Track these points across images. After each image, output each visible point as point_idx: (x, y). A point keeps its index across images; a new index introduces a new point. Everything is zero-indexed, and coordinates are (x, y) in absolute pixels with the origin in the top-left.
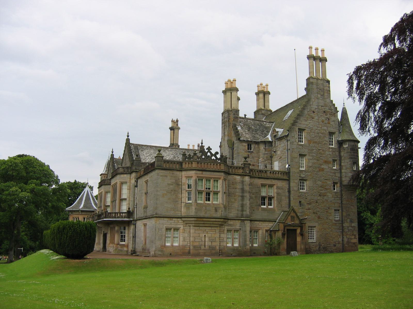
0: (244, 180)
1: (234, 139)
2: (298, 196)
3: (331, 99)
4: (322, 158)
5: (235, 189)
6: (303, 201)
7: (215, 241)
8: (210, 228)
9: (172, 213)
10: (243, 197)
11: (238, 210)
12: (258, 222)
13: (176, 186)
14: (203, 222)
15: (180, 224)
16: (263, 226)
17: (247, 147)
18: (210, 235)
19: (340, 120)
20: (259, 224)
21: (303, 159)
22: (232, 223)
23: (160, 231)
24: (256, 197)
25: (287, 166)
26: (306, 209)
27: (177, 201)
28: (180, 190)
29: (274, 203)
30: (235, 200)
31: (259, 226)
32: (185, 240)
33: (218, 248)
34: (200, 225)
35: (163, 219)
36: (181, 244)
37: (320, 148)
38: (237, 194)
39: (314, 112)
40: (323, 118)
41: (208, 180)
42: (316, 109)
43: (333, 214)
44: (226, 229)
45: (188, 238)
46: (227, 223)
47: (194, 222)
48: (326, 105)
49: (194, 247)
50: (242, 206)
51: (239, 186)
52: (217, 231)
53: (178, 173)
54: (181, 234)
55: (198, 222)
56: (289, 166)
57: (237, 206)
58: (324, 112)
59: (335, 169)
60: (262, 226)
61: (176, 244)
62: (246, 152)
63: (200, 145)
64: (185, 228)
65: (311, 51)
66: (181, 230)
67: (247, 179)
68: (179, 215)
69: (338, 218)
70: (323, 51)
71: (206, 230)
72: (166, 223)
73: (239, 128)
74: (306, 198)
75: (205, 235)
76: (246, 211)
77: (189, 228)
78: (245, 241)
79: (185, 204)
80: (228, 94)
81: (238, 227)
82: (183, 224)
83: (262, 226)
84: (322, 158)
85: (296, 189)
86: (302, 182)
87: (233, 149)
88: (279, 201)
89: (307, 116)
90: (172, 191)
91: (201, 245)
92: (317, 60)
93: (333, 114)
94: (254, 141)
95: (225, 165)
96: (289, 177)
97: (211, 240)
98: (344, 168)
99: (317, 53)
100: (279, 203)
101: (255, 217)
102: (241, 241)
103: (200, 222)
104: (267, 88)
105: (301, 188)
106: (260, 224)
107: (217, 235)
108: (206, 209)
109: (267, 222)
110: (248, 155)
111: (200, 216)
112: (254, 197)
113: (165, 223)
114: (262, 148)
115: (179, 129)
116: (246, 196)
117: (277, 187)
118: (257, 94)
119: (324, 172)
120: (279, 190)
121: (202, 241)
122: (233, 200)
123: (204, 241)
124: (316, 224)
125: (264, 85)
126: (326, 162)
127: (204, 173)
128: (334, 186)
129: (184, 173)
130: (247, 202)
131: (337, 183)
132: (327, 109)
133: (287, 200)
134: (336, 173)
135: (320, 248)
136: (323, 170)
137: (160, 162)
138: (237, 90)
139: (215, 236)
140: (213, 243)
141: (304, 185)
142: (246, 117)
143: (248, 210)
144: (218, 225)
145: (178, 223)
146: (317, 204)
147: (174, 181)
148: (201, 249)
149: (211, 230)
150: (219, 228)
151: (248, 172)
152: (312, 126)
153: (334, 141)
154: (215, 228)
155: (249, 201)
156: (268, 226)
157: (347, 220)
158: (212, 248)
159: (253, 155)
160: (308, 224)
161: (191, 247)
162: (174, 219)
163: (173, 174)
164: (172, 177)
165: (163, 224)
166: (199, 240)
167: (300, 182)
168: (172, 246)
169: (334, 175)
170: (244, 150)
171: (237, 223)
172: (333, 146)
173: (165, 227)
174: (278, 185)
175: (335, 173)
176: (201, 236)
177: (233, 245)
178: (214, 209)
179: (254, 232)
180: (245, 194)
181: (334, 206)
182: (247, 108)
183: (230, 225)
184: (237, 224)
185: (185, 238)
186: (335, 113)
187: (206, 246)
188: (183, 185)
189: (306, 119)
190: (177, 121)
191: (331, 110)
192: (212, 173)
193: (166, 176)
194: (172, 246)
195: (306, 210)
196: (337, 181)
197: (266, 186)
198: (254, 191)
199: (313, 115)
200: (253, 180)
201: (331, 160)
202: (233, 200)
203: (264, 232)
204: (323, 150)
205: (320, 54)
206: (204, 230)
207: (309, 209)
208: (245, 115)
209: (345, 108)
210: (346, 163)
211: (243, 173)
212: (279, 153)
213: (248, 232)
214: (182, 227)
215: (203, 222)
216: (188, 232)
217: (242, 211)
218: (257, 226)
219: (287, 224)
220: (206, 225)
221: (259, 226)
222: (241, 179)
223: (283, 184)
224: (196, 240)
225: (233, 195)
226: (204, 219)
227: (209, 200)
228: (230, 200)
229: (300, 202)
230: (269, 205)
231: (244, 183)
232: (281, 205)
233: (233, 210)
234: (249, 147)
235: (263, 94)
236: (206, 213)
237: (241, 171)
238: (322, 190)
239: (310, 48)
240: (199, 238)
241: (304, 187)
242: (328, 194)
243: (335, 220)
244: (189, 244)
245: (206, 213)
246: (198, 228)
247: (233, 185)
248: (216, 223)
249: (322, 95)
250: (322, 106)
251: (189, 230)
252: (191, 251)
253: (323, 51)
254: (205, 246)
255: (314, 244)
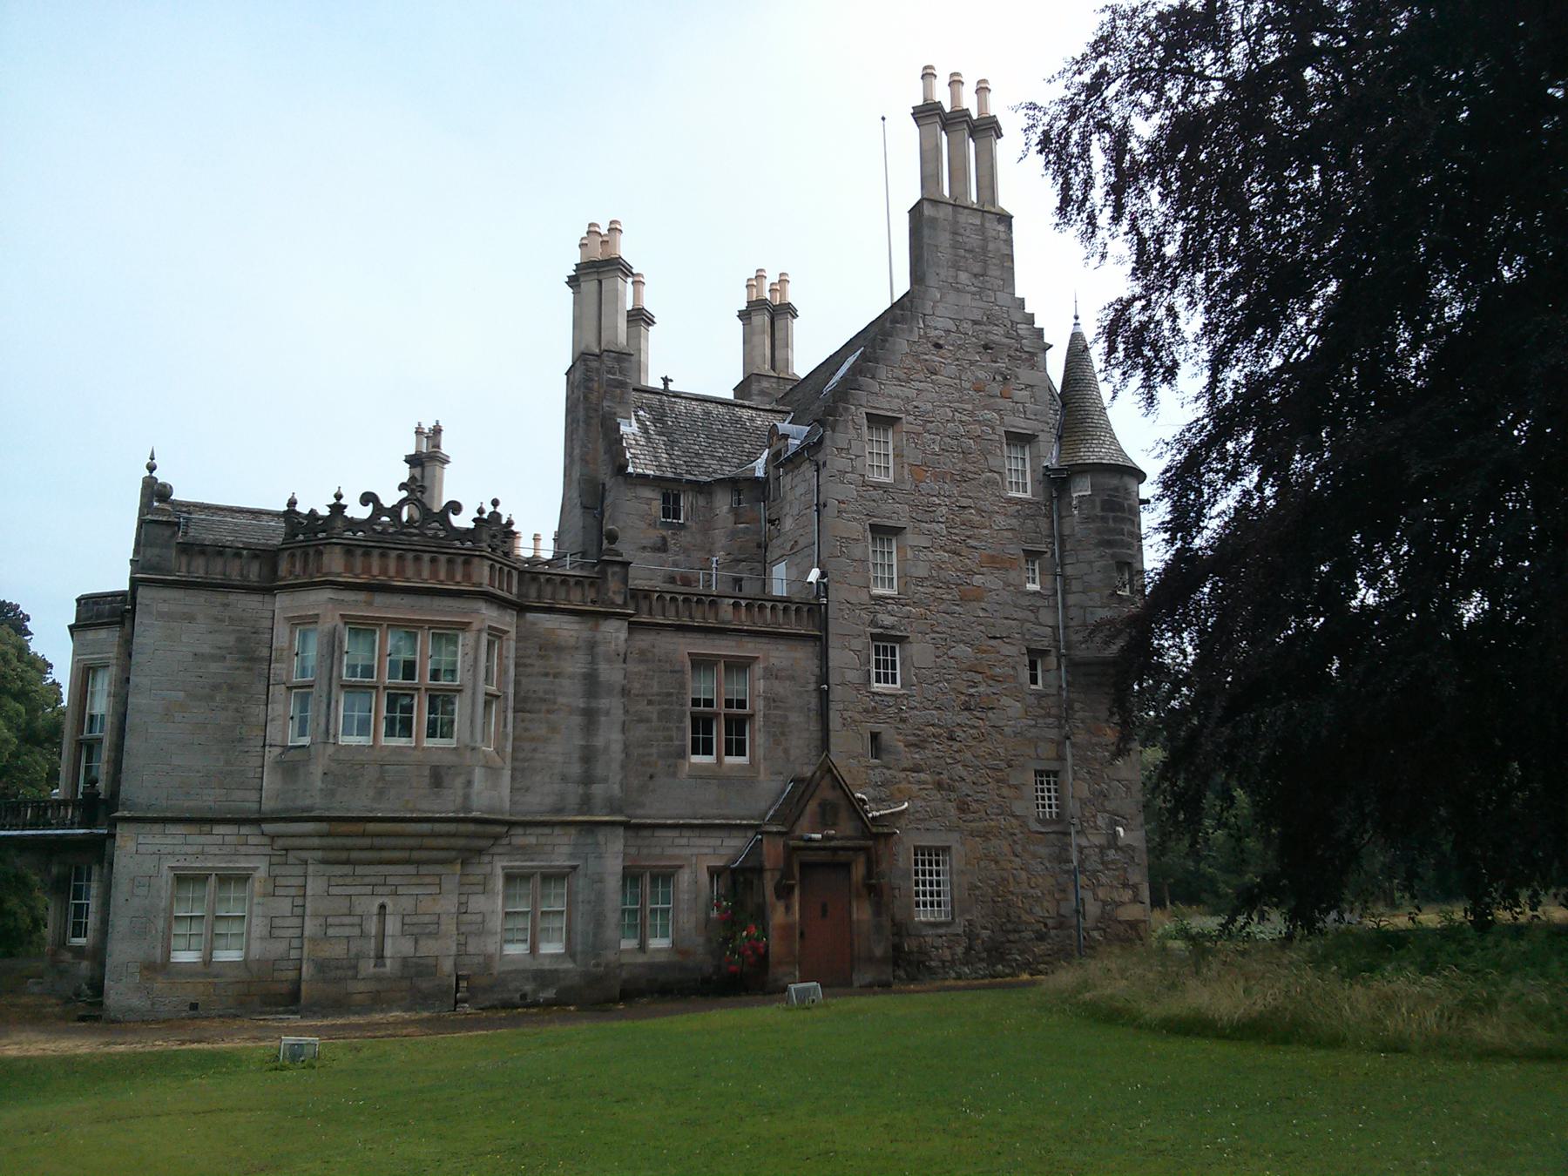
0: (599, 637)
1: (604, 474)
2: (866, 711)
3: (1017, 295)
4: (972, 542)
5: (550, 679)
6: (889, 735)
7: (434, 935)
8: (411, 869)
9: (208, 799)
10: (590, 717)
11: (564, 778)
12: (675, 833)
13: (238, 664)
14: (367, 842)
15: (252, 850)
16: (695, 851)
17: (657, 506)
18: (407, 904)
19: (1058, 386)
20: (677, 841)
21: (890, 546)
22: (533, 840)
23: (142, 891)
24: (664, 715)
25: (814, 575)
26: (904, 770)
27: (241, 740)
28: (261, 687)
29: (752, 740)
30: (553, 729)
31: (677, 851)
32: (277, 933)
33: (447, 966)
34: (355, 855)
35: (157, 828)
36: (257, 949)
37: (965, 502)
38: (562, 700)
39: (938, 346)
40: (981, 374)
41: (410, 628)
42: (948, 331)
43: (1029, 791)
44: (499, 872)
45: (296, 922)
46: (505, 841)
47: (316, 842)
48: (991, 319)
49: (322, 966)
50: (588, 756)
51: (574, 665)
52: (450, 884)
53: (250, 604)
54: (255, 900)
55: (339, 841)
56: (823, 575)
57: (560, 759)
58: (986, 347)
59: (1035, 593)
60: (688, 851)
61: (228, 955)
62: (652, 525)
63: (489, 509)
64: (278, 870)
65: (927, 89)
66: (257, 885)
67: (614, 633)
68: (245, 801)
69: (1054, 809)
70: (982, 89)
71: (390, 880)
72: (177, 849)
73: (629, 428)
74: (903, 720)
75: (383, 907)
76: (605, 780)
77: (298, 870)
78: (598, 921)
79: (277, 751)
80: (589, 286)
81: (561, 860)
82: (267, 850)
83: (688, 851)
84: (972, 542)
85: (853, 676)
86: (885, 648)
87: (602, 514)
88: (779, 731)
89: (909, 362)
90: (216, 688)
91: (358, 957)
92: (953, 126)
93: (1024, 356)
94: (688, 481)
95: (498, 566)
96: (824, 627)
97: (416, 930)
98: (1076, 586)
99: (955, 97)
100: (777, 743)
101: (654, 809)
102: (579, 926)
103: (349, 842)
104: (783, 293)
105: (878, 674)
106: (684, 841)
107: (448, 904)
108: (382, 778)
109: (717, 833)
110: (664, 538)
111: (348, 810)
112: (655, 716)
113: (170, 849)
114: (725, 508)
115: (445, 461)
116: (607, 713)
117: (765, 669)
118: (744, 316)
119: (983, 605)
120: (776, 683)
121: (363, 935)
122: (542, 731)
123: (373, 932)
124: (952, 840)
125: (772, 277)
126: (996, 562)
127: (379, 599)
128: (1033, 666)
129: (284, 603)
130: (610, 737)
131: (1044, 653)
132: (997, 335)
133: (814, 727)
134: (1042, 611)
135: (969, 948)
136: (977, 595)
137: (156, 551)
138: (625, 270)
139: (437, 909)
140: (421, 943)
141: (894, 662)
142: (672, 387)
143: (616, 778)
144: (454, 854)
145: (243, 849)
146: (956, 746)
147: (231, 640)
148: (355, 978)
149: (415, 880)
150: (458, 867)
151: (619, 600)
152: (929, 406)
153: (1033, 471)
154: (439, 869)
155: (623, 731)
156: (722, 851)
157: (1094, 816)
158: (415, 969)
159: (685, 538)
160: (908, 840)
161: (307, 970)
162: (219, 829)
163: (226, 605)
164: (223, 621)
165: (159, 854)
166: (347, 931)
167: (877, 648)
168: (208, 962)
169: (1032, 617)
170: (642, 518)
171: (558, 841)
172: (1028, 495)
173: (172, 868)
174: (772, 660)
175: (1035, 610)
176: (358, 911)
177: (533, 949)
178: (427, 772)
179: (654, 879)
180: (603, 703)
181: (1032, 753)
182: (695, 356)
183: (523, 850)
184: (560, 851)
185: (278, 922)
186: (1033, 355)
187: (388, 962)
188: (277, 661)
189: (900, 373)
190: (437, 431)
191: (1019, 338)
192: (425, 601)
193: (191, 618)
194: (208, 962)
195: (903, 775)
196: (1043, 644)
197: (716, 663)
198: (656, 689)
199: (935, 358)
200: (644, 640)
201: (1015, 550)
202: (542, 731)
203: (704, 878)
204: (980, 511)
205: (969, 102)
206: (380, 880)
207: (916, 769)
208: (666, 380)
209: (1080, 334)
210: (1089, 564)
211: (593, 602)
212: (788, 524)
213: (613, 883)
214: (261, 867)
215: (367, 842)
216: (293, 891)
217: (587, 780)
218: (669, 851)
219: (801, 838)
220: (386, 855)
221: (677, 851)
222: (586, 634)
223: (800, 658)
224: (331, 932)
225: (544, 707)
226: (371, 827)
227: (406, 730)
228: (526, 730)
229: (875, 736)
230: (729, 753)
231: (601, 649)
232: (786, 751)
233: (538, 778)
234: (671, 508)
235: (768, 315)
236: (380, 793)
237: (576, 599)
238: (975, 685)
239: (928, 74)
240: (347, 920)
241: (894, 668)
242: (1005, 701)
243: (1039, 821)
244: (294, 954)
245: (380, 793)
246: (347, 869)
247: (542, 657)
248: (442, 842)
249: (975, 275)
250: (975, 322)
251: (300, 881)
252: (304, 987)
253: (982, 89)
254: (380, 957)
255: (942, 931)
